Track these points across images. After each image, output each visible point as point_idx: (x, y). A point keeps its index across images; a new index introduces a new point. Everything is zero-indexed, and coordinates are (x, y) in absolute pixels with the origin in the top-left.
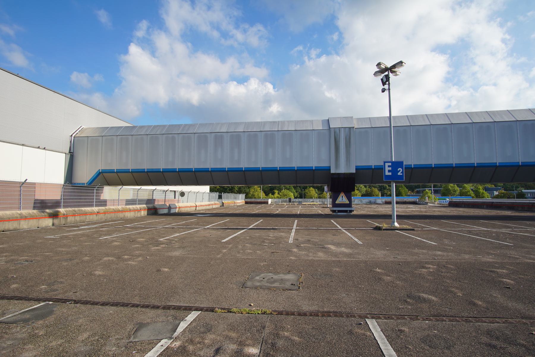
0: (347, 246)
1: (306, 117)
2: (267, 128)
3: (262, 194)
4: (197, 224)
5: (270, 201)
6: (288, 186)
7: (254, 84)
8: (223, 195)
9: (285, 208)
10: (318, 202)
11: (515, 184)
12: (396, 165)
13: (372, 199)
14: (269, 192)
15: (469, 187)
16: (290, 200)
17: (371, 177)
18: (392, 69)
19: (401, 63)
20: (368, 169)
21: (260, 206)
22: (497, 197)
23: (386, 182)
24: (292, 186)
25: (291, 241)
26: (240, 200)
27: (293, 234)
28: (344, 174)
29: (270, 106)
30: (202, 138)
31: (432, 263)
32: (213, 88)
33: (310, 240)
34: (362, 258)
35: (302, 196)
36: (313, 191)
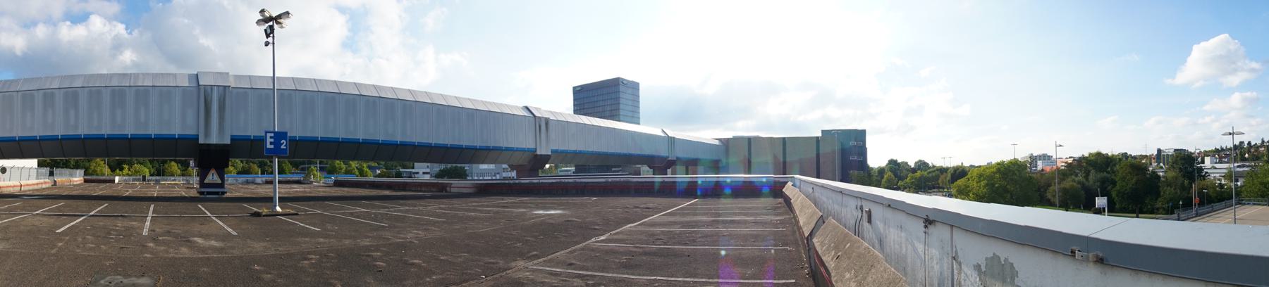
0: (217, 238)
1: (172, 69)
2: (115, 83)
3: (107, 170)
4: (23, 208)
5: (117, 179)
6: (141, 159)
7: (97, 23)
8: (56, 171)
9: (137, 188)
10: (180, 181)
11: (395, 163)
12: (279, 136)
13: (249, 177)
14: (116, 167)
15: (354, 164)
16: (144, 178)
17: (248, 150)
18: (276, 19)
19: (288, 13)
20: (246, 140)
21: (103, 186)
22: (379, 176)
23: (268, 157)
24: (147, 159)
25: (145, 232)
26: (77, 178)
27: (148, 223)
28: (216, 145)
29: (121, 53)
30: (28, 97)
31: (314, 253)
32: (41, 31)
33: (158, 219)
34: (236, 252)
35: (160, 172)
36: (174, 167)
